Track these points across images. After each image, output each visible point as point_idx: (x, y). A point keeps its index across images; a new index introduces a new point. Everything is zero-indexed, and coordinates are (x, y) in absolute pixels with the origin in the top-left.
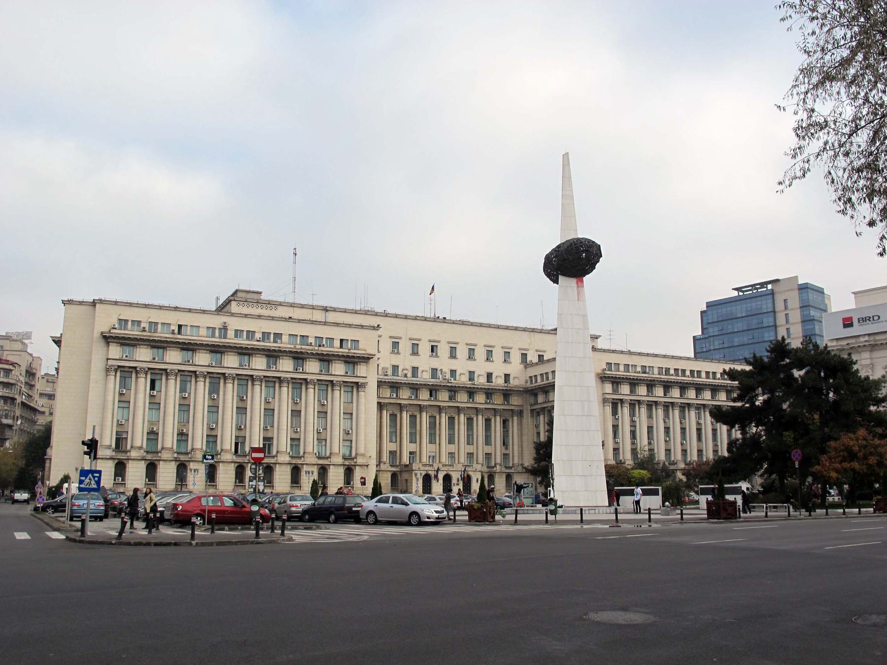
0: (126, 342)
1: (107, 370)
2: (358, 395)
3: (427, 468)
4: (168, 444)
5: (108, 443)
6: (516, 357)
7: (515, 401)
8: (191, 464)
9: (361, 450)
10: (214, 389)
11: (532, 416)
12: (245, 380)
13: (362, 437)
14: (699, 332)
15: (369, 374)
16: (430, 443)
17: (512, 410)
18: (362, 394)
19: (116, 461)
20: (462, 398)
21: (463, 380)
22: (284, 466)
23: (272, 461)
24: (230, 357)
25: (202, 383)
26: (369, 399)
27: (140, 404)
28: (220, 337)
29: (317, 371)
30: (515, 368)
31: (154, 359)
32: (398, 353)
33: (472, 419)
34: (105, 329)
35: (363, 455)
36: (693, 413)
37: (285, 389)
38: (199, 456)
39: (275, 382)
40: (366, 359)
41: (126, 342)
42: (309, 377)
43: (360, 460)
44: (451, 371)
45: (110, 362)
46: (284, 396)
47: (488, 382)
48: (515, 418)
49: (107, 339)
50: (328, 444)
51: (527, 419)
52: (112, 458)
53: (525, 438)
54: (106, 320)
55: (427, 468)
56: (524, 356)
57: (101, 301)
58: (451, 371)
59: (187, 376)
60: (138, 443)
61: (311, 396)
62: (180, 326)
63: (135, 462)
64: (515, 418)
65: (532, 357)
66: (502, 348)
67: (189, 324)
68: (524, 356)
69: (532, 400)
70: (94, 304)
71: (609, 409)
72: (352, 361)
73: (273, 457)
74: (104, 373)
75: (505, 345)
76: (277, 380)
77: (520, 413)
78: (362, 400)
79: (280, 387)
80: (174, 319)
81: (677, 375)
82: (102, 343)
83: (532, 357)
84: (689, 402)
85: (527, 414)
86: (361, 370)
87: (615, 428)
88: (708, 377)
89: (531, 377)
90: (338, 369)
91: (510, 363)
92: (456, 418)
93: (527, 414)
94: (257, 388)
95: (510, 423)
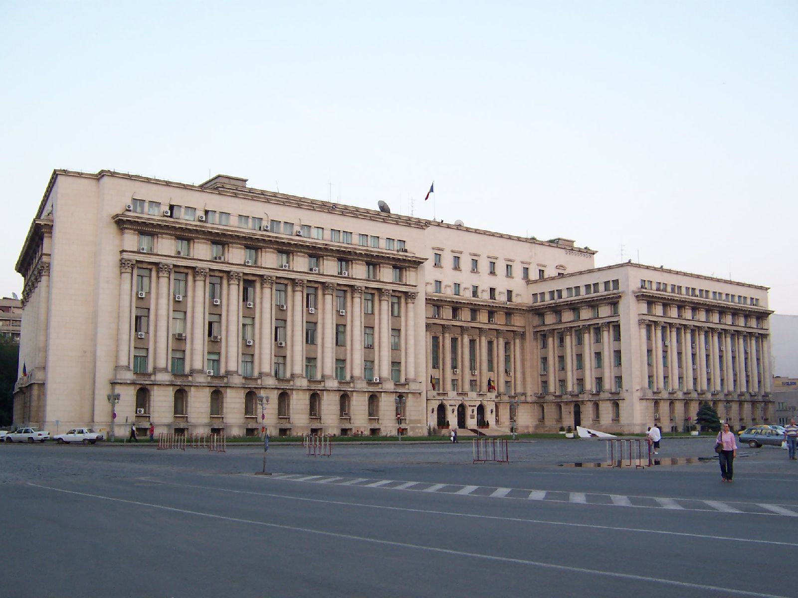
0: (146, 229)
1: (123, 263)
2: (407, 308)
3: (441, 398)
4: (198, 365)
5: (126, 364)
6: (518, 271)
7: (518, 321)
8: (228, 390)
9: (411, 375)
10: (309, 302)
11: (536, 339)
12: (346, 291)
13: (411, 359)
14: (249, 185)
15: (422, 282)
16: (434, 367)
17: (461, 327)
18: (410, 306)
19: (138, 387)
20: (500, 319)
21: (467, 295)
22: (332, 394)
23: (320, 387)
24: (235, 250)
25: (166, 280)
26: (416, 316)
27: (163, 312)
28: (678, 294)
29: (364, 276)
30: (517, 284)
31: (179, 253)
32: (477, 272)
33: (457, 339)
34: (119, 210)
35: (415, 381)
36: (729, 340)
37: (267, 291)
38: (237, 380)
39: (151, 270)
40: (417, 263)
41: (146, 229)
42: (357, 283)
43: (413, 387)
44: (491, 289)
45: (126, 256)
46: (356, 308)
47: (491, 298)
48: (517, 341)
49: (121, 223)
50: (376, 367)
51: (532, 346)
52: (133, 383)
53: (528, 364)
54: (117, 200)
55: (441, 398)
56: (526, 270)
57: (113, 174)
58: (491, 289)
59: (217, 278)
60: (162, 363)
61: (328, 304)
62: (207, 212)
63: (162, 388)
64: (517, 341)
65: (534, 275)
66: (538, 265)
67: (218, 210)
68: (526, 270)
69: (536, 321)
70: (102, 175)
71: (644, 332)
72: (404, 264)
73: (320, 382)
74: (117, 270)
75: (456, 249)
76: (225, 276)
77: (523, 336)
78: (411, 314)
79: (262, 288)
80: (166, 197)
81: (701, 297)
82: (113, 228)
83: (534, 275)
84: (352, 283)
85: (529, 336)
86: (410, 277)
87: (649, 351)
88: (687, 294)
89: (535, 295)
90: (387, 274)
91: (442, 267)
92: (460, 339)
93: (529, 336)
94: (164, 281)
95: (512, 347)
